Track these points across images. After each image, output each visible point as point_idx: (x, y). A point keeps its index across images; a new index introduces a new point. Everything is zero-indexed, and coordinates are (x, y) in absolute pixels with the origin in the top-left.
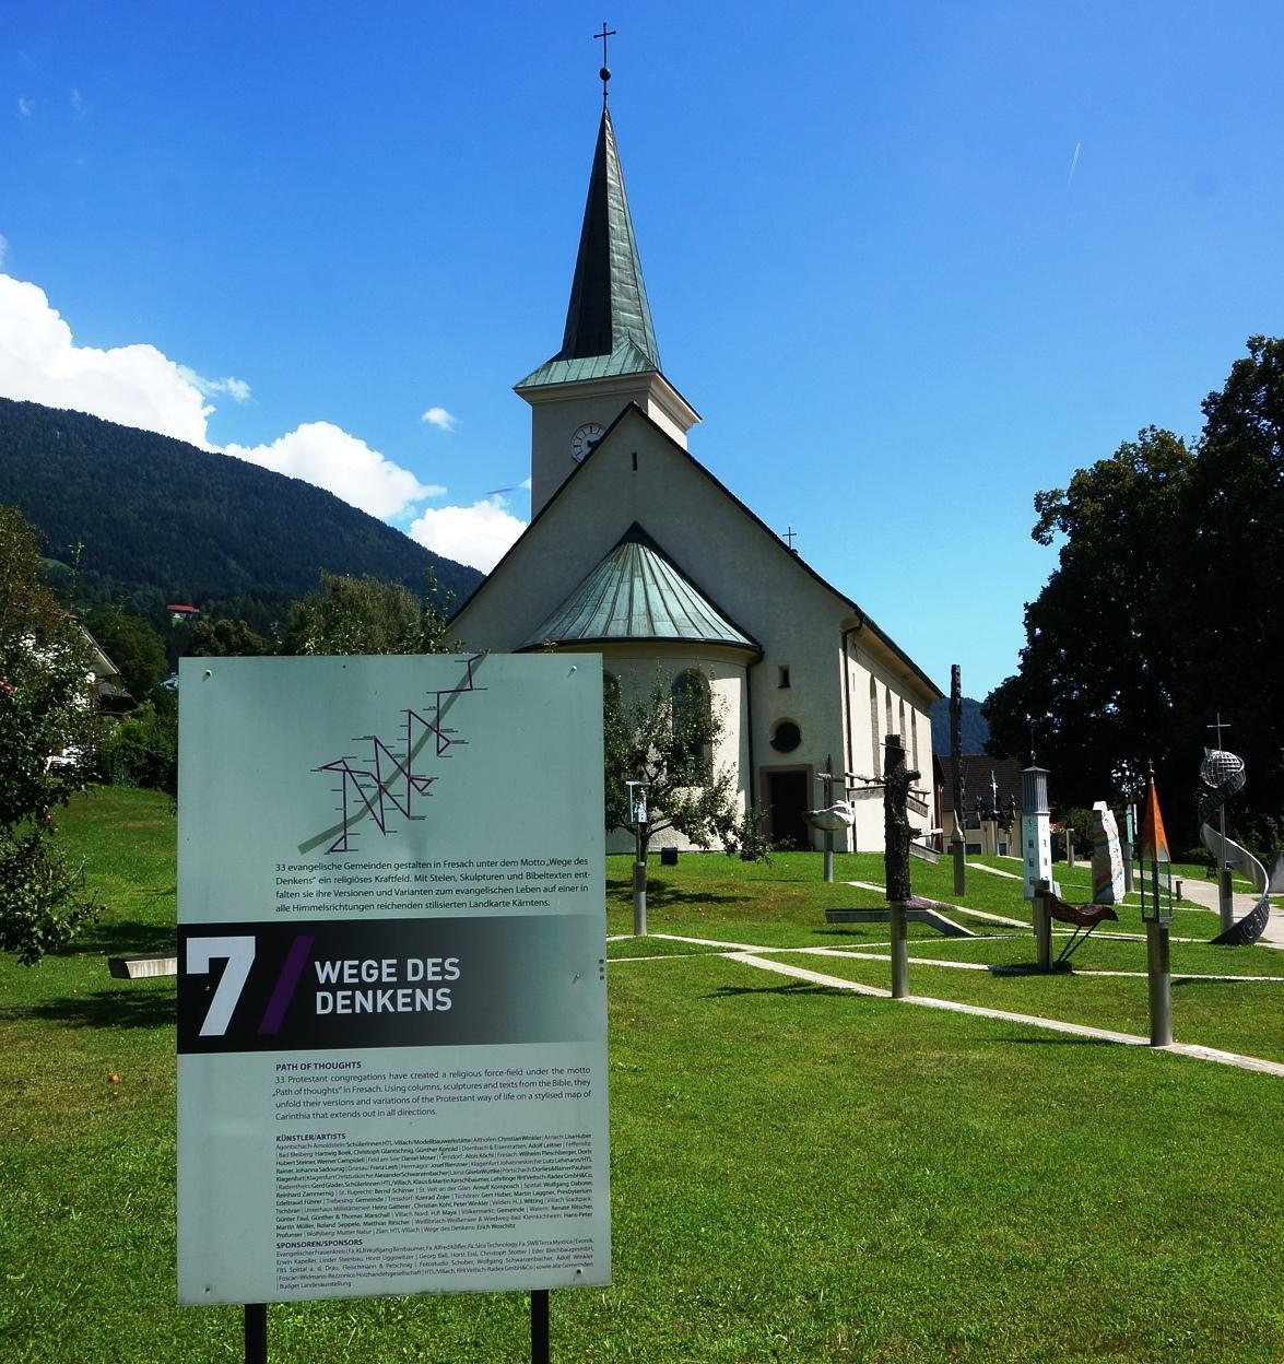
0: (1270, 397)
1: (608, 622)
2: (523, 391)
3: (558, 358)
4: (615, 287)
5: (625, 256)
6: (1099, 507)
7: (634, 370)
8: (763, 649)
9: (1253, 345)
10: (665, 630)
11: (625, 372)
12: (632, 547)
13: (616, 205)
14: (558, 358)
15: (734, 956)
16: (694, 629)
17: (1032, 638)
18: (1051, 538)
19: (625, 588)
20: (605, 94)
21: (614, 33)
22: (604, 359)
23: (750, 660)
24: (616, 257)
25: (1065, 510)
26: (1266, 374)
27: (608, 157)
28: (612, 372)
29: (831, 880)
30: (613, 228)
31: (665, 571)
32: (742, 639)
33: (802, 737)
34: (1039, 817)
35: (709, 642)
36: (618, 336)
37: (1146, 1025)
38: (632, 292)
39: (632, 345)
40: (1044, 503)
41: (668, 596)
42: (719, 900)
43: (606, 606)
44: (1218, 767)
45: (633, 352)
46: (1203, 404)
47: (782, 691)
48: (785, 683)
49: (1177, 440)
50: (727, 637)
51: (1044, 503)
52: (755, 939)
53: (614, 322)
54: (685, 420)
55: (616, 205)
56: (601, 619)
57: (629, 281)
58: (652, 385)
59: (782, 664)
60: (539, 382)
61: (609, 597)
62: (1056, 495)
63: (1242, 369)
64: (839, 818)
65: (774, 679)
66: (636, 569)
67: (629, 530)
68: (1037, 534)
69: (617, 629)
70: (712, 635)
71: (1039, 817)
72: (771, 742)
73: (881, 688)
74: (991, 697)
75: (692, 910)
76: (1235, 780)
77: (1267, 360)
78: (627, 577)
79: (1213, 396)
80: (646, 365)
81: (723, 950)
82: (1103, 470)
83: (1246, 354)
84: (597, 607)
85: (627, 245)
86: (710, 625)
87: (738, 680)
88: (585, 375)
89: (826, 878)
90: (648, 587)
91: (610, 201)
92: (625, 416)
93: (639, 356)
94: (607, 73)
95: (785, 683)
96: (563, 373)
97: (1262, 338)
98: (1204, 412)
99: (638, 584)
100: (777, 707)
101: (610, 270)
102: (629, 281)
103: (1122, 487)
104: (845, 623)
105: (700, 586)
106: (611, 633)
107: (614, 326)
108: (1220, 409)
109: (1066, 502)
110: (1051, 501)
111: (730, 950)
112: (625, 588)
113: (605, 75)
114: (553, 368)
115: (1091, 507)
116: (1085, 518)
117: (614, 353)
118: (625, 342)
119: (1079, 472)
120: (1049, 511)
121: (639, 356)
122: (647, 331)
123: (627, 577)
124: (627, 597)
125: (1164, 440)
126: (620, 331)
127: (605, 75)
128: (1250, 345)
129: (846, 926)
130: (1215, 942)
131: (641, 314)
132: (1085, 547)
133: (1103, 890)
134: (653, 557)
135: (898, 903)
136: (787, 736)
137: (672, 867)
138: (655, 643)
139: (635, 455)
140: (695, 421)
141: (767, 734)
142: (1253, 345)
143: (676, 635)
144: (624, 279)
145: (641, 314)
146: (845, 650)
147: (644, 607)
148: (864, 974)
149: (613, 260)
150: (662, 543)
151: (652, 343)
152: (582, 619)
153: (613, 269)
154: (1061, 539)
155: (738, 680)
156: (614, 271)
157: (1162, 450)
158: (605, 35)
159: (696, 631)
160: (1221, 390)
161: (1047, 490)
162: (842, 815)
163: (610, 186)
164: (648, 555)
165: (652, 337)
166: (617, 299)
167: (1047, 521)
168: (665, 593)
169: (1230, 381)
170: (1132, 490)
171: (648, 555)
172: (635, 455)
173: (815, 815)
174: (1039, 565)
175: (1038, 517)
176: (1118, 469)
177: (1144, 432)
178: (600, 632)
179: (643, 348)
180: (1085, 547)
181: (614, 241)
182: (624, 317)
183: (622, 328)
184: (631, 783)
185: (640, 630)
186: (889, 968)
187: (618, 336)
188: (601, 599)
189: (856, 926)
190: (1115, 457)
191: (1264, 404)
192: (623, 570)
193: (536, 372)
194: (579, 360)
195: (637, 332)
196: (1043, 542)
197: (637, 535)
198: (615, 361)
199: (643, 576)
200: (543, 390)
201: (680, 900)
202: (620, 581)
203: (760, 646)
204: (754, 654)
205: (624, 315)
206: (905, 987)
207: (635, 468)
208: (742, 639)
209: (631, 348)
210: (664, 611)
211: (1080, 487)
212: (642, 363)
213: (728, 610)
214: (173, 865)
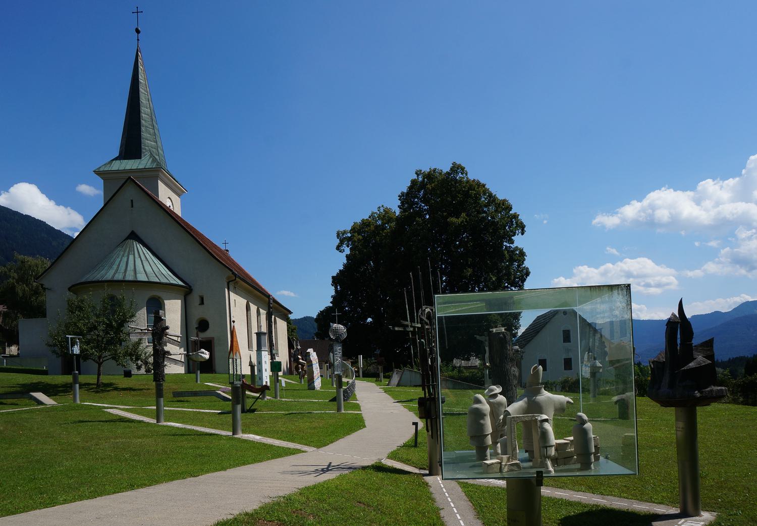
0: (425, 194)
1: (115, 274)
2: (98, 173)
3: (116, 159)
4: (143, 129)
5: (148, 115)
6: (360, 237)
7: (151, 167)
8: (192, 288)
9: (418, 173)
10: (142, 277)
11: (147, 167)
12: (130, 241)
13: (143, 91)
14: (116, 159)
15: (109, 410)
16: (156, 278)
17: (336, 291)
18: (344, 250)
19: (125, 259)
20: (138, 40)
21: (142, 12)
22: (138, 161)
23: (186, 292)
24: (143, 115)
25: (349, 239)
26: (423, 185)
27: (140, 69)
28: (141, 167)
29: (199, 382)
30: (142, 102)
31: (145, 252)
32: (181, 283)
33: (210, 326)
34: (263, 352)
35: (166, 284)
36: (144, 151)
37: (231, 429)
38: (151, 132)
39: (151, 155)
40: (341, 235)
41: (146, 264)
42: (134, 390)
43: (115, 267)
44: (336, 331)
45: (151, 159)
46: (399, 196)
47: (200, 306)
48: (202, 303)
49: (393, 211)
50: (172, 282)
51: (341, 235)
52: (108, 403)
53: (142, 145)
54: (180, 192)
55: (143, 91)
56: (111, 272)
57: (150, 127)
58: (160, 174)
59: (201, 295)
60: (106, 169)
61: (117, 263)
62: (345, 232)
63: (414, 182)
64: (201, 356)
65: (197, 301)
66: (131, 251)
67: (130, 234)
68: (338, 248)
69: (119, 277)
70: (164, 280)
71: (263, 352)
72: (196, 328)
73: (253, 308)
74: (319, 315)
75: (672, 442)
76: (341, 336)
77: (424, 179)
78: (126, 254)
79: (403, 194)
80: (157, 165)
81: (105, 408)
82: (365, 224)
83: (415, 177)
84: (111, 267)
85: (149, 110)
86: (161, 273)
87: (180, 301)
88: (128, 167)
89: (197, 381)
90: (136, 259)
91: (140, 89)
92: (127, 183)
93: (154, 160)
94: (139, 30)
95: (202, 303)
96: (118, 166)
97: (421, 171)
98: (399, 199)
99: (131, 257)
100: (198, 313)
101: (140, 121)
102: (150, 127)
103: (370, 229)
104: (228, 278)
105: (163, 260)
106: (115, 279)
107: (143, 147)
108: (407, 199)
109: (349, 235)
110: (343, 234)
111: (108, 408)
112: (125, 259)
113: (138, 31)
114: (112, 164)
115: (358, 237)
116: (355, 241)
117: (143, 159)
118: (148, 154)
119: (355, 223)
120: (343, 239)
121: (154, 160)
122: (159, 149)
123: (126, 254)
124: (125, 263)
125: (387, 211)
126: (145, 149)
127: (138, 31)
128: (416, 173)
129: (182, 399)
130: (330, 401)
131: (156, 142)
132: (355, 254)
133: (311, 384)
134: (140, 246)
135: (158, 383)
136: (203, 325)
137: (129, 378)
138: (136, 283)
139: (132, 201)
140: (183, 192)
141: (194, 324)
142: (418, 173)
143: (147, 280)
144: (148, 125)
145: (156, 142)
146: (228, 289)
147: (132, 268)
148: (147, 414)
149: (142, 117)
150: (146, 241)
151: (161, 155)
152: (103, 272)
153: (142, 121)
154: (347, 251)
155: (180, 301)
156: (143, 122)
157: (386, 215)
158: (137, 12)
159: (157, 279)
160: (405, 191)
161: (342, 230)
162: (202, 355)
163: (141, 82)
164: (138, 245)
165: (162, 153)
166: (144, 134)
167: (342, 243)
168: (144, 262)
169: (409, 188)
170: (374, 231)
171: (138, 245)
172: (132, 201)
173: (190, 355)
174: (338, 261)
175: (338, 241)
176: (370, 222)
177: (379, 208)
178: (111, 276)
179: (157, 157)
180: (355, 254)
181: (143, 108)
182: (148, 143)
183: (147, 148)
184: (70, 336)
185: (130, 277)
186: (155, 412)
187: (144, 151)
188: (113, 264)
189: (186, 398)
190: (369, 218)
191: (422, 198)
192: (125, 251)
193: (105, 165)
194: (126, 161)
195: (154, 150)
196: (340, 252)
197: (134, 236)
198: (143, 162)
199: (134, 254)
200: (107, 173)
201: (64, 385)
202: (123, 256)
203: (190, 287)
204: (187, 290)
205: (147, 141)
206: (162, 418)
207: (132, 206)
208: (181, 283)
209: (150, 157)
210: (142, 270)
211: (355, 230)
212: (155, 164)
213: (176, 270)
214: (203, 407)
